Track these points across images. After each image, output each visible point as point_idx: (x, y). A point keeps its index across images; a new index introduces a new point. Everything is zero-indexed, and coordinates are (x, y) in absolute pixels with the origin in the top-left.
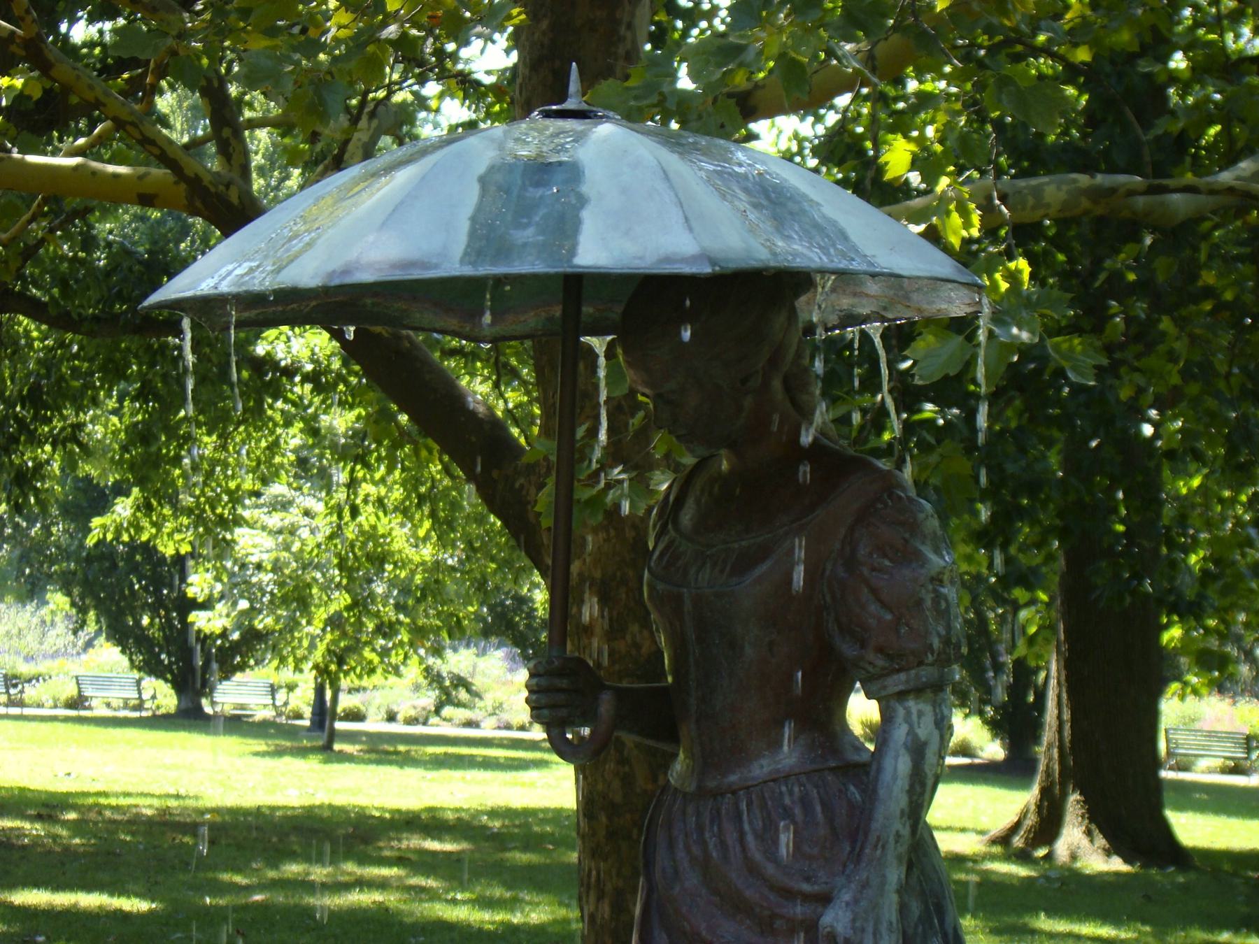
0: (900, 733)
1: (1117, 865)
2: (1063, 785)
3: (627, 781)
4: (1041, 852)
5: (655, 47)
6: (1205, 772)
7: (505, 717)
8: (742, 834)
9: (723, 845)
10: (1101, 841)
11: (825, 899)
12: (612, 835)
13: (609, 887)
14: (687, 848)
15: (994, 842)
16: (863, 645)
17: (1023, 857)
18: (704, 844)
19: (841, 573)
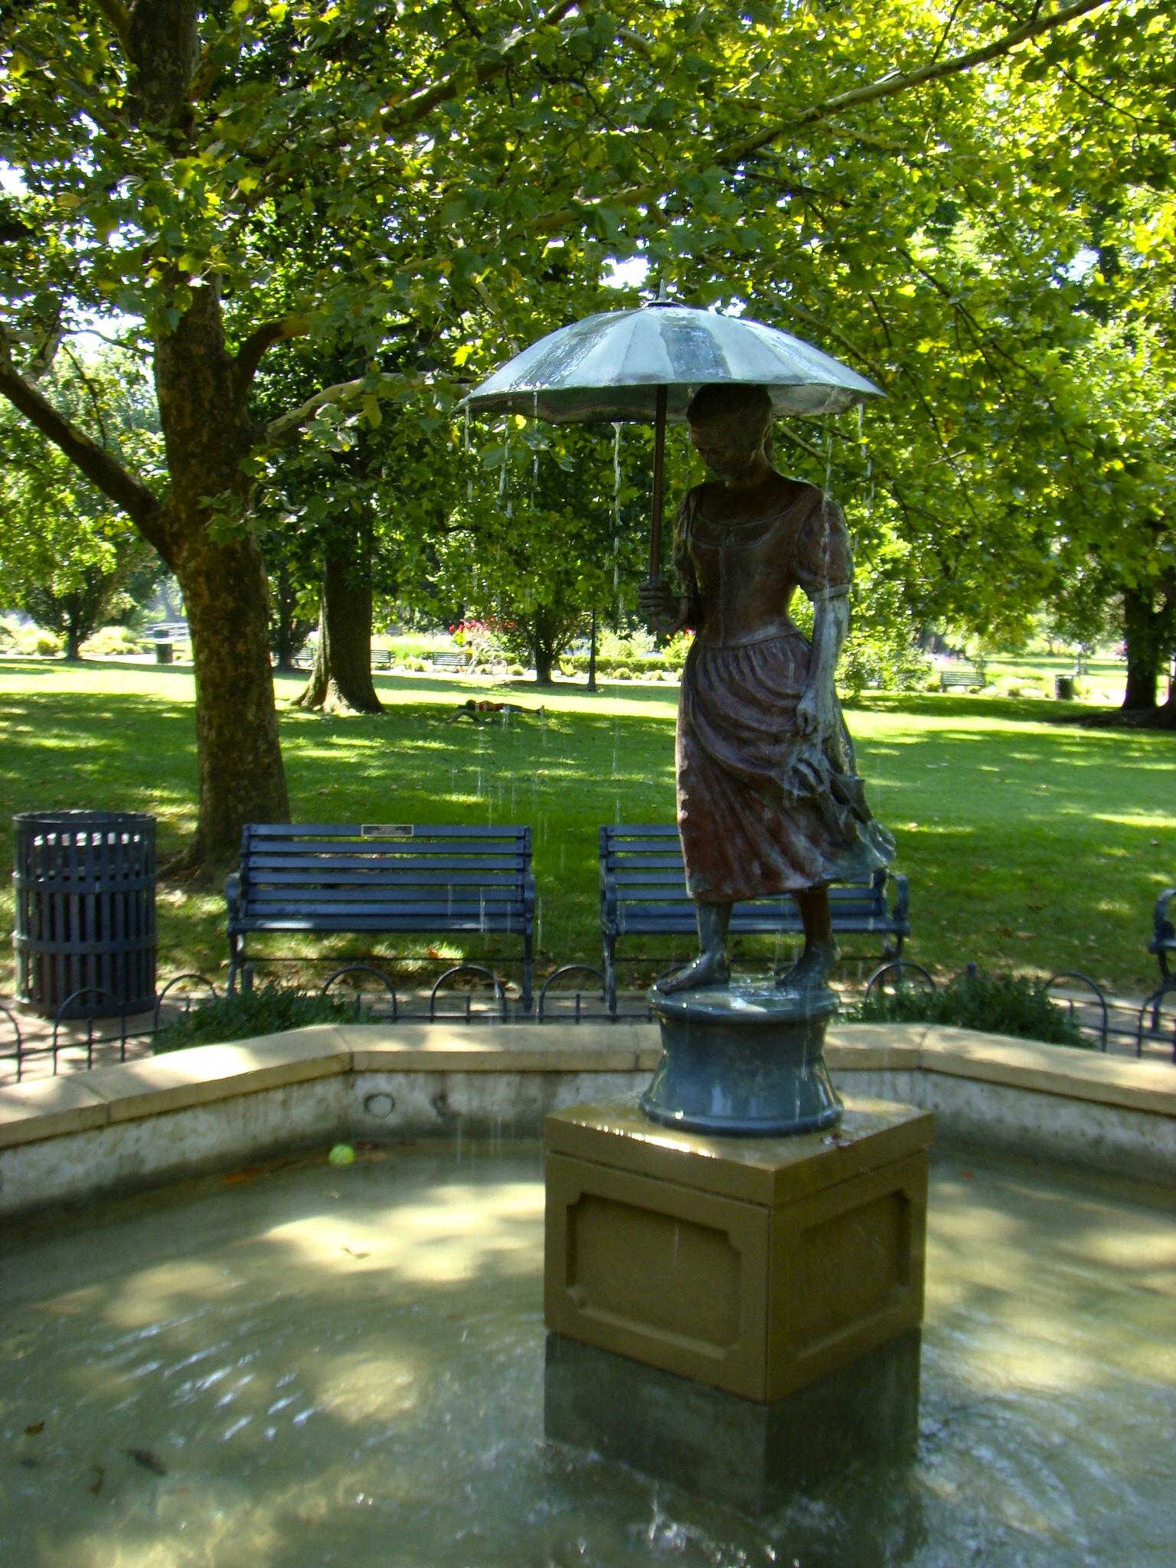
0: (830, 617)
1: (353, 712)
2: (326, 676)
3: (223, 671)
4: (317, 708)
5: (440, 274)
6: (398, 670)
7: (20, 649)
8: (752, 669)
9: (741, 672)
10: (345, 702)
11: (798, 697)
12: (216, 698)
13: (215, 723)
14: (719, 676)
15: (293, 704)
16: (816, 574)
17: (309, 710)
18: (730, 674)
19: (803, 537)
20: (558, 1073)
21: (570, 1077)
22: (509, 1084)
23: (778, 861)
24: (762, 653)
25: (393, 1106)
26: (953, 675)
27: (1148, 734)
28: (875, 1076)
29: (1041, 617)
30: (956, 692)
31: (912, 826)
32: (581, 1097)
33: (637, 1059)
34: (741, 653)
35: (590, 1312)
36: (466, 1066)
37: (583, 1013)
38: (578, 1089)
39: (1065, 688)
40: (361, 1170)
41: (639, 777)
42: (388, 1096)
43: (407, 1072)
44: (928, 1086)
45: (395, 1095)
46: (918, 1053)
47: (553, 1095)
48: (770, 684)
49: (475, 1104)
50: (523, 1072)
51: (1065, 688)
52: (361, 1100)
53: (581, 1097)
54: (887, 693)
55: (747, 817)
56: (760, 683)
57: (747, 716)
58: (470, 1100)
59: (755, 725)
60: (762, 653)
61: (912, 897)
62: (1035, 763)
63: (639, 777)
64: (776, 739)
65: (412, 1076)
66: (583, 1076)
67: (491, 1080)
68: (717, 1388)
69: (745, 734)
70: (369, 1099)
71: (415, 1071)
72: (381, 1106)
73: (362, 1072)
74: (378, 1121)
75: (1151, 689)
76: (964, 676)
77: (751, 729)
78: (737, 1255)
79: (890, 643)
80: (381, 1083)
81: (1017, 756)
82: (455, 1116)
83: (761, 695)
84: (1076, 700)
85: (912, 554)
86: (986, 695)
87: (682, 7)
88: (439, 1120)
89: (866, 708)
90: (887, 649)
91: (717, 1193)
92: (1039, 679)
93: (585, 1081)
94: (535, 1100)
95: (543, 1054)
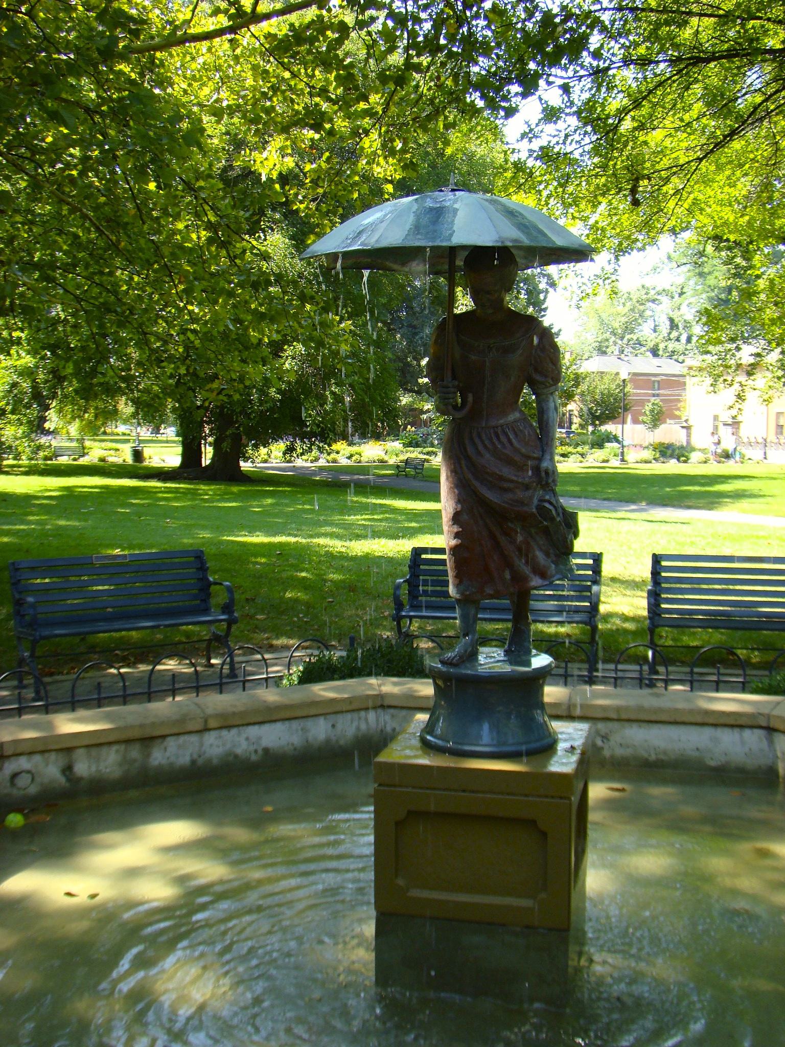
9: (503, 444)
20: (152, 738)
21: (160, 740)
22: (117, 751)
23: (527, 570)
24: (514, 430)
25: (33, 779)
26: (61, 448)
27: (204, 484)
28: (355, 715)
29: (125, 407)
30: (64, 460)
31: (117, 551)
32: (168, 754)
33: (206, 721)
34: (499, 430)
35: (415, 893)
36: (87, 742)
37: (128, 692)
38: (165, 749)
39: (138, 455)
40: (31, 831)
41: (62, 523)
42: (28, 772)
43: (43, 752)
44: (387, 718)
45: (34, 771)
46: (381, 696)
47: (149, 755)
48: (523, 450)
49: (94, 769)
50: (128, 742)
51: (138, 455)
52: (8, 778)
53: (168, 754)
54: (21, 462)
55: (503, 540)
56: (517, 450)
57: (506, 471)
58: (89, 767)
59: (515, 478)
60: (514, 430)
61: (237, 596)
62: (149, 505)
63: (62, 523)
64: (527, 487)
65: (47, 755)
66: (169, 739)
67: (104, 750)
68: (527, 927)
69: (506, 485)
70: (15, 776)
71: (50, 751)
72: (24, 781)
73: (8, 757)
74: (22, 792)
75: (199, 454)
76: (68, 448)
77: (512, 481)
78: (544, 835)
79: (22, 427)
80: (23, 763)
81: (134, 501)
82: (80, 779)
83: (517, 458)
84: (146, 463)
85: (37, 367)
86: (83, 461)
87: (759, 3)
88: (67, 785)
89: (7, 473)
90: (21, 431)
91: (552, 797)
92: (117, 450)
93: (171, 743)
94: (135, 761)
95: (141, 726)
